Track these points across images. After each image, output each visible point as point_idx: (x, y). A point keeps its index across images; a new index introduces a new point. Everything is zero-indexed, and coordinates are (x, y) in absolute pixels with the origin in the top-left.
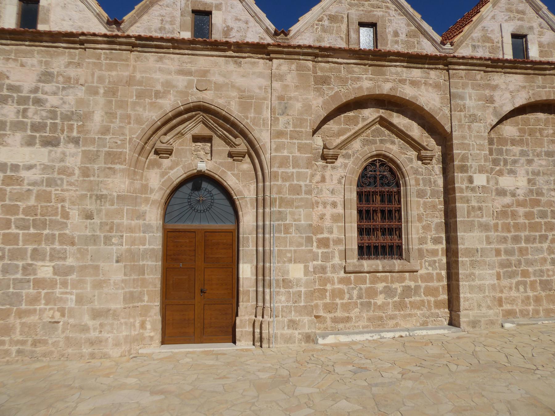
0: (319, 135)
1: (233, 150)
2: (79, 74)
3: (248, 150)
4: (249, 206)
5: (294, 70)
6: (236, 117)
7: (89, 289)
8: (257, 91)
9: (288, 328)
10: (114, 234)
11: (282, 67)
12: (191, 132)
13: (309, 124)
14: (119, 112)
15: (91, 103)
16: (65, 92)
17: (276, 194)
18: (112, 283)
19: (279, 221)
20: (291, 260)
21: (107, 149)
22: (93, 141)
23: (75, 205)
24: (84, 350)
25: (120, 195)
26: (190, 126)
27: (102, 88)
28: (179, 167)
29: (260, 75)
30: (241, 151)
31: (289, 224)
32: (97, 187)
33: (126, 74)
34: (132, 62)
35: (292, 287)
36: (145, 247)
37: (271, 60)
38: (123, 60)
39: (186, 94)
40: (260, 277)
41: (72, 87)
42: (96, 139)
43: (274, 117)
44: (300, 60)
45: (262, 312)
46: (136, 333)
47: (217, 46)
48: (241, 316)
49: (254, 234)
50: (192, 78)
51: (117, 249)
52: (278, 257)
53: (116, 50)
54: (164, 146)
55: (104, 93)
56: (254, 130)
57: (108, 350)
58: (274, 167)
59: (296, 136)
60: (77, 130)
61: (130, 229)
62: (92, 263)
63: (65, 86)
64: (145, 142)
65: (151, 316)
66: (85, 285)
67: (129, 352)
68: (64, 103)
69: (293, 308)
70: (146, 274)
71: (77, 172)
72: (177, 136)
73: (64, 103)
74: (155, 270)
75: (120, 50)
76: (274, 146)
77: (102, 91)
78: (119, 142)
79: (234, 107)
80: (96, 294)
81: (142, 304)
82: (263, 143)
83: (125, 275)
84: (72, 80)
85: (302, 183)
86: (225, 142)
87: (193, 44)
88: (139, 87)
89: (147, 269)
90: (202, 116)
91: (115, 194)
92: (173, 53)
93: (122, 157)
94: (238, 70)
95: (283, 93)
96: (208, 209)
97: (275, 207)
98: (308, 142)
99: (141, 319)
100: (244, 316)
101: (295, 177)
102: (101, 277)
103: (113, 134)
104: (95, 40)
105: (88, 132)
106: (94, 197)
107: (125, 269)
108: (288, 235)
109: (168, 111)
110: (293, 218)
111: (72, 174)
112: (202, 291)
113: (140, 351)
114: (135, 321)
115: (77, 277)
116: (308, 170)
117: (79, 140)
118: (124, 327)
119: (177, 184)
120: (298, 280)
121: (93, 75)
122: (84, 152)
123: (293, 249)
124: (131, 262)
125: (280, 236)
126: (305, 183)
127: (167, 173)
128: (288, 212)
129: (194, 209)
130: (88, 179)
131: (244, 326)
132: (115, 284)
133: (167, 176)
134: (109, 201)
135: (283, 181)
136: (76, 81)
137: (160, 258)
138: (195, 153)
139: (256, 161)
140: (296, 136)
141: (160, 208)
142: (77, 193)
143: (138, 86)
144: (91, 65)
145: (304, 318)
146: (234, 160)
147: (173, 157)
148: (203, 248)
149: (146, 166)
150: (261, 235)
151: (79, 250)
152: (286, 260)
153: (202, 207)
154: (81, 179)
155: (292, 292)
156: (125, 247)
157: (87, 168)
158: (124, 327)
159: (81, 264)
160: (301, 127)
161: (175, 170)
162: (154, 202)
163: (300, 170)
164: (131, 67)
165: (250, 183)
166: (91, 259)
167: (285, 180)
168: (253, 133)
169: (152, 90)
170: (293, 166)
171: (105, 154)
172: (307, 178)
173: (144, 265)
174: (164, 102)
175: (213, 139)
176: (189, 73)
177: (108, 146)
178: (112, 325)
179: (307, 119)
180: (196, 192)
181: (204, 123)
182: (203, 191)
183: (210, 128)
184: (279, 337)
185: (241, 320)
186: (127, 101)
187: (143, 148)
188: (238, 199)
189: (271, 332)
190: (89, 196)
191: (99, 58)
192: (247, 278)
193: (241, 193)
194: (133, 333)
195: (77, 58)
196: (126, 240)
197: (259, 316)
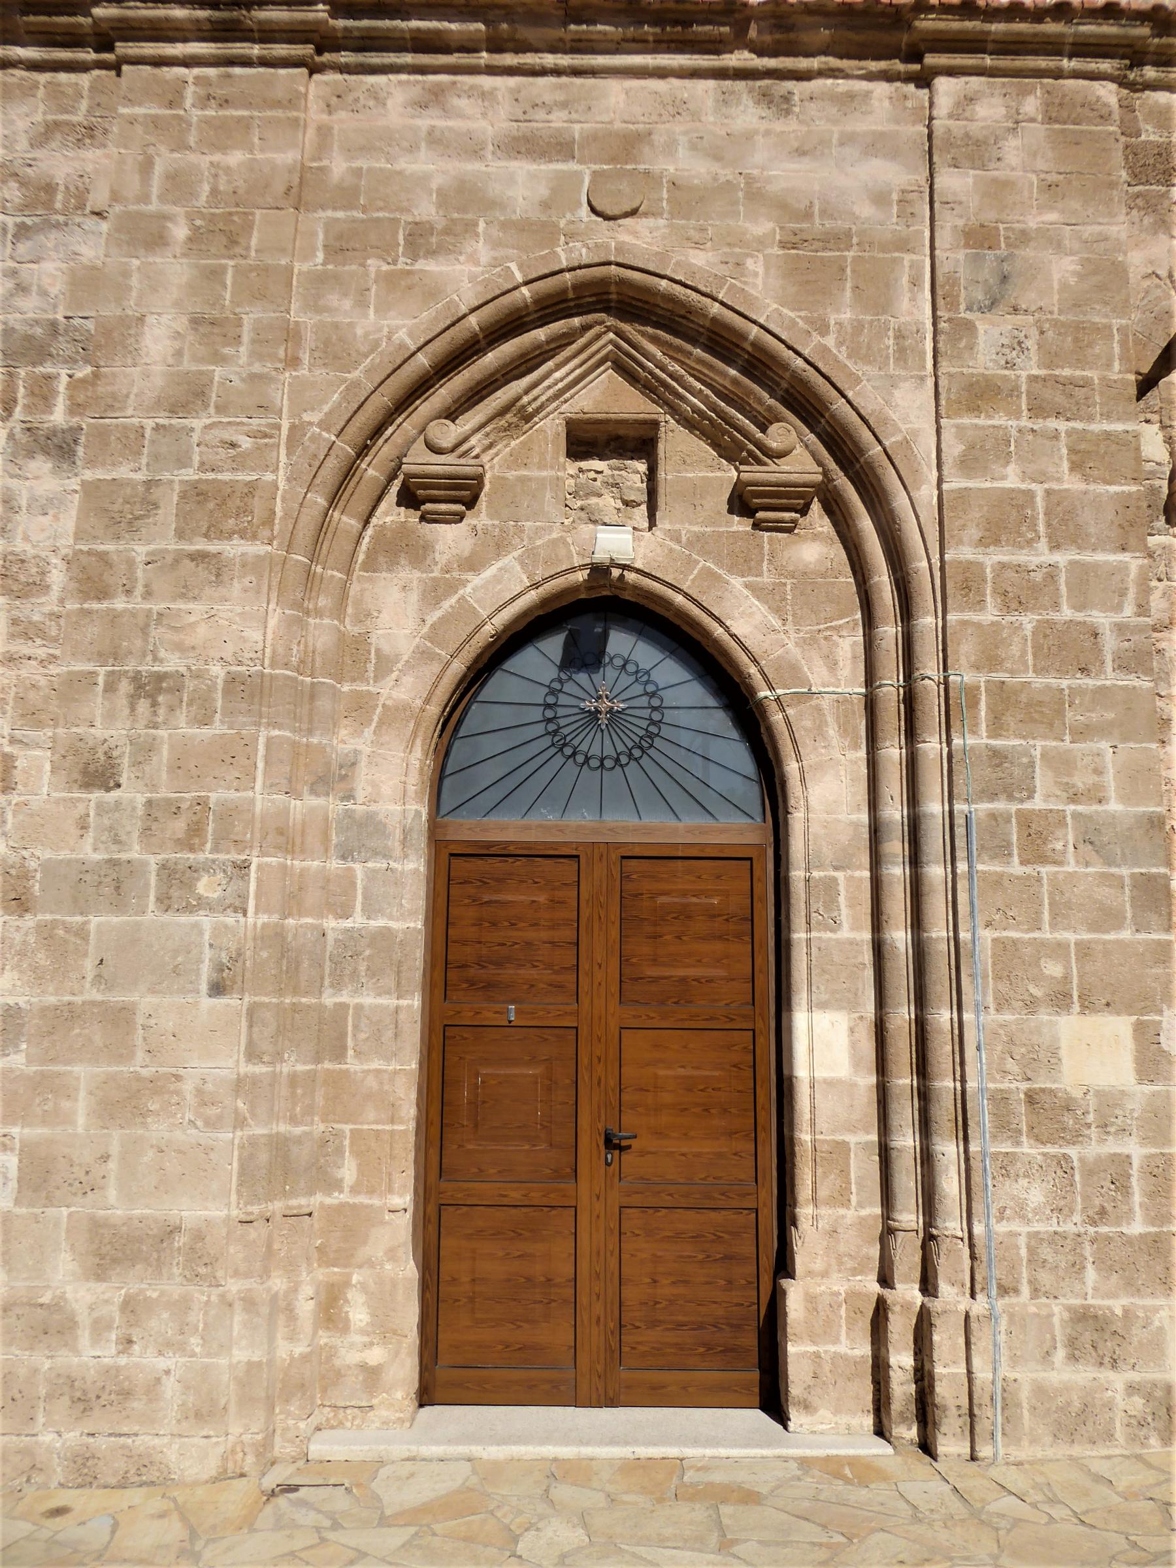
0: (1149, 416)
1: (753, 473)
2: (89, 168)
3: (825, 473)
4: (832, 731)
5: (1033, 120)
6: (772, 327)
7: (81, 1120)
8: (866, 210)
9: (1073, 1358)
10: (205, 855)
11: (978, 108)
12: (564, 408)
13: (1117, 349)
14: (252, 316)
15: (134, 281)
16: (29, 244)
17: (977, 667)
18: (190, 1098)
19: (993, 796)
20: (1067, 995)
21: (190, 474)
22: (132, 442)
23: (39, 725)
24: (47, 1438)
25: (240, 674)
26: (558, 375)
27: (182, 221)
28: (509, 560)
29: (876, 146)
30: (794, 478)
31: (1045, 814)
32: (139, 643)
33: (288, 157)
34: (314, 114)
35: (1076, 1137)
36: (348, 924)
37: (924, 80)
38: (277, 104)
39: (545, 232)
40: (904, 1081)
41: (57, 226)
42: (148, 433)
43: (950, 320)
44: (1058, 74)
45: (917, 1258)
46: (300, 1349)
47: (687, 24)
48: (810, 1273)
49: (859, 868)
50: (572, 166)
51: (218, 930)
52: (998, 978)
53: (246, 62)
54: (440, 465)
55: (190, 239)
56: (858, 381)
57: (156, 1441)
58: (960, 542)
59: (1060, 399)
60: (71, 398)
61: (281, 832)
62: (99, 997)
63: (28, 221)
64: (359, 441)
65: (369, 1263)
66: (65, 1104)
67: (259, 1455)
68: (22, 289)
69: (1088, 1250)
70: (350, 1052)
71: (57, 577)
72: (503, 422)
73: (22, 289)
74: (390, 1034)
75: (265, 62)
76: (953, 449)
77: (180, 232)
78: (246, 443)
79: (759, 281)
80: (115, 1149)
81: (328, 1201)
82: (899, 438)
83: (252, 1054)
84: (60, 197)
85: (1102, 619)
86: (715, 445)
87: (579, 22)
88: (340, 214)
89: (355, 1027)
90: (611, 335)
91: (218, 671)
92: (492, 70)
93: (257, 505)
94: (779, 126)
95: (989, 216)
96: (637, 753)
97: (974, 732)
98: (1119, 427)
99: (322, 1274)
100: (825, 1274)
101: (1063, 589)
102: (140, 1066)
103: (220, 409)
104: (159, 20)
105: (113, 404)
106: (125, 687)
107: (250, 1026)
108: (1046, 870)
109: (464, 309)
110: (1067, 787)
111: (39, 586)
112: (610, 1143)
113: (317, 1449)
114: (295, 1290)
115: (29, 1062)
116: (1125, 557)
117: (75, 441)
118: (238, 1318)
119: (498, 636)
120: (1110, 1101)
121: (146, 166)
122: (90, 490)
123: (1070, 937)
124: (280, 992)
125: (1001, 875)
126: (1117, 618)
127: (453, 587)
128: (1037, 753)
129: (574, 754)
130: (104, 605)
131: (828, 1332)
132: (204, 1099)
133: (453, 600)
134: (190, 703)
135: (1006, 608)
136: (76, 197)
137: (418, 975)
138: (579, 503)
139: (866, 524)
140: (1060, 399)
141: (419, 742)
142: (54, 669)
143: (335, 209)
144: (139, 129)
145: (1149, 1302)
146: (756, 526)
147: (481, 517)
148: (615, 933)
149: (361, 557)
150: (897, 872)
151: (46, 933)
152: (1037, 992)
153: (607, 742)
154: (72, 606)
155: (1081, 1160)
156: (255, 919)
157: (102, 557)
158: (238, 1318)
159: (52, 1000)
160: (1081, 363)
161: (489, 572)
162: (393, 715)
163: (1087, 557)
164: (311, 133)
165: (837, 629)
166: (99, 976)
167: (1014, 605)
168: (850, 394)
169: (396, 221)
170: (1050, 537)
171: (183, 496)
172: (1123, 593)
173: (344, 1007)
174: (443, 268)
175: (662, 434)
176: (562, 148)
177: (196, 459)
178: (183, 1305)
179: (1110, 327)
180: (582, 677)
181: (620, 368)
182: (611, 673)
183: (649, 387)
184: (1025, 1405)
185: (811, 1300)
186: (289, 270)
187: (349, 472)
188: (778, 700)
189: (983, 1374)
190: (101, 680)
191: (174, 102)
192: (830, 1083)
193: (794, 672)
194: (287, 1350)
195: (84, 105)
196: (258, 886)
197: (907, 1280)
